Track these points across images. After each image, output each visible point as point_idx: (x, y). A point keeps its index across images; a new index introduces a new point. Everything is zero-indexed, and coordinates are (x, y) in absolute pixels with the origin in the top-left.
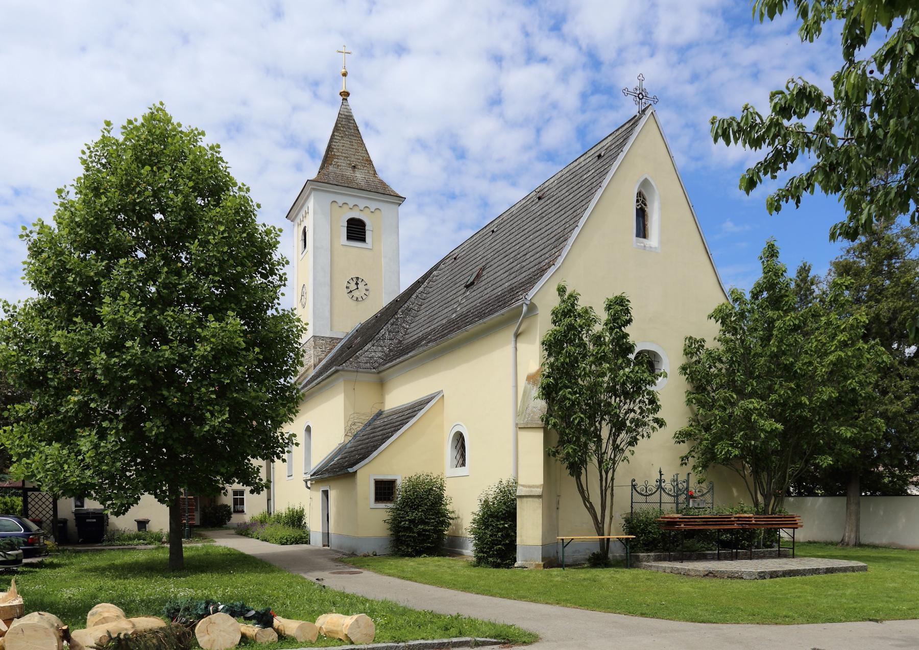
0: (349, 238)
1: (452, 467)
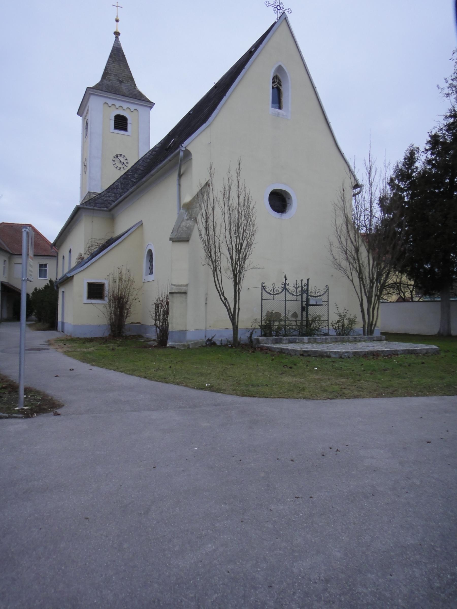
0: (116, 127)
1: (146, 275)
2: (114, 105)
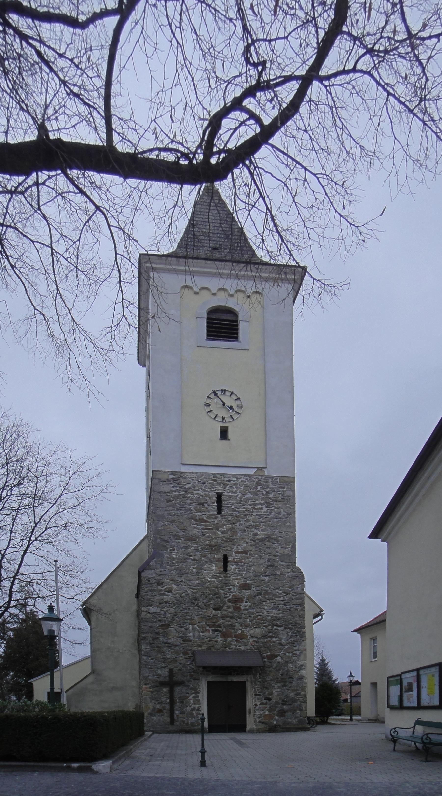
2: (207, 289)
